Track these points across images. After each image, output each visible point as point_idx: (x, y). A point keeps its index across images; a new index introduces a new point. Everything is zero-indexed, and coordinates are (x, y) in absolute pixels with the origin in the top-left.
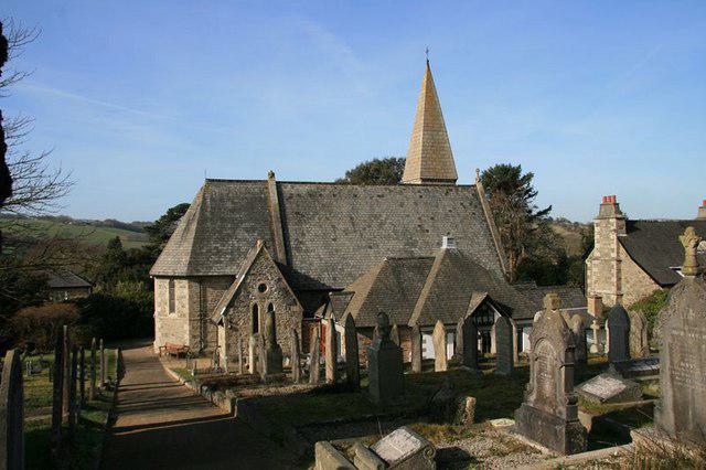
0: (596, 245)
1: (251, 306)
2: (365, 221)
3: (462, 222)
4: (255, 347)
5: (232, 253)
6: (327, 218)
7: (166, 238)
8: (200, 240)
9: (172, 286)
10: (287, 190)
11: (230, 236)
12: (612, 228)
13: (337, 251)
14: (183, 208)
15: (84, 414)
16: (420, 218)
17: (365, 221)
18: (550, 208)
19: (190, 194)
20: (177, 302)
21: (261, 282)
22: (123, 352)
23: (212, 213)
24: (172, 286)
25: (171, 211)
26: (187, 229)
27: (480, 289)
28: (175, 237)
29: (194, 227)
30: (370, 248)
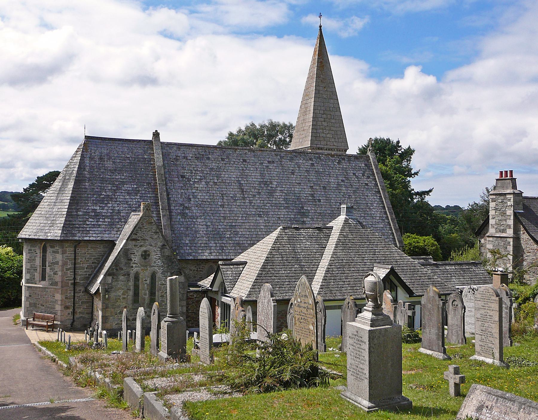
0: (492, 222)
1: (132, 276)
2: (255, 188)
3: (355, 192)
4: (44, 353)
5: (111, 217)
6: (215, 184)
7: (34, 206)
8: (74, 201)
9: (44, 251)
10: (173, 153)
11: (109, 198)
12: (509, 203)
13: (225, 218)
14: (52, 176)
15: (205, 303)
16: (311, 187)
17: (255, 188)
18: (430, 191)
19: (60, 154)
20: (48, 269)
21: (145, 249)
22: (284, 102)
23: (90, 172)
24: (44, 251)
25: (40, 179)
26: (61, 190)
27: (383, 262)
28: (43, 207)
29: (71, 185)
30: (260, 216)
